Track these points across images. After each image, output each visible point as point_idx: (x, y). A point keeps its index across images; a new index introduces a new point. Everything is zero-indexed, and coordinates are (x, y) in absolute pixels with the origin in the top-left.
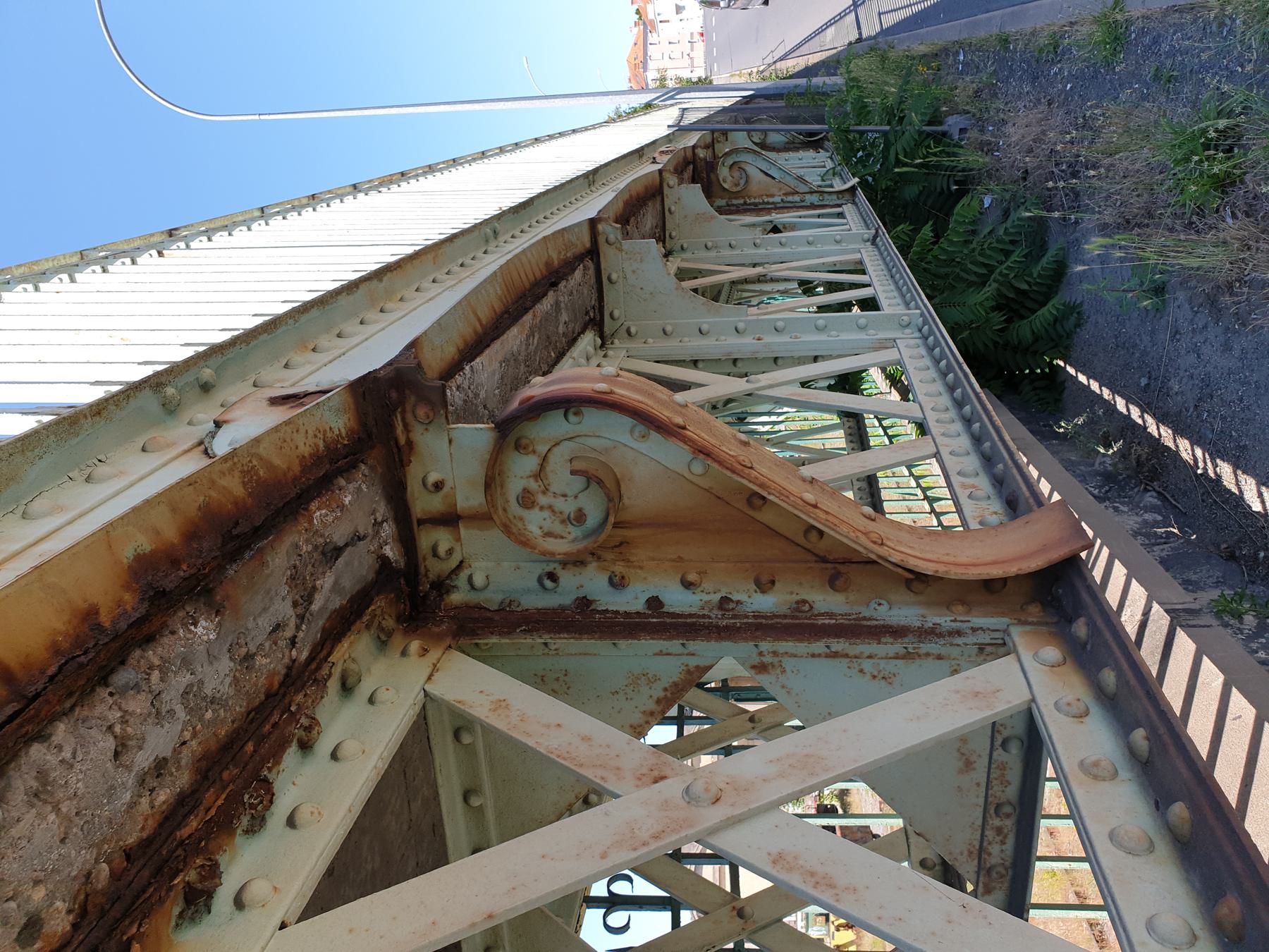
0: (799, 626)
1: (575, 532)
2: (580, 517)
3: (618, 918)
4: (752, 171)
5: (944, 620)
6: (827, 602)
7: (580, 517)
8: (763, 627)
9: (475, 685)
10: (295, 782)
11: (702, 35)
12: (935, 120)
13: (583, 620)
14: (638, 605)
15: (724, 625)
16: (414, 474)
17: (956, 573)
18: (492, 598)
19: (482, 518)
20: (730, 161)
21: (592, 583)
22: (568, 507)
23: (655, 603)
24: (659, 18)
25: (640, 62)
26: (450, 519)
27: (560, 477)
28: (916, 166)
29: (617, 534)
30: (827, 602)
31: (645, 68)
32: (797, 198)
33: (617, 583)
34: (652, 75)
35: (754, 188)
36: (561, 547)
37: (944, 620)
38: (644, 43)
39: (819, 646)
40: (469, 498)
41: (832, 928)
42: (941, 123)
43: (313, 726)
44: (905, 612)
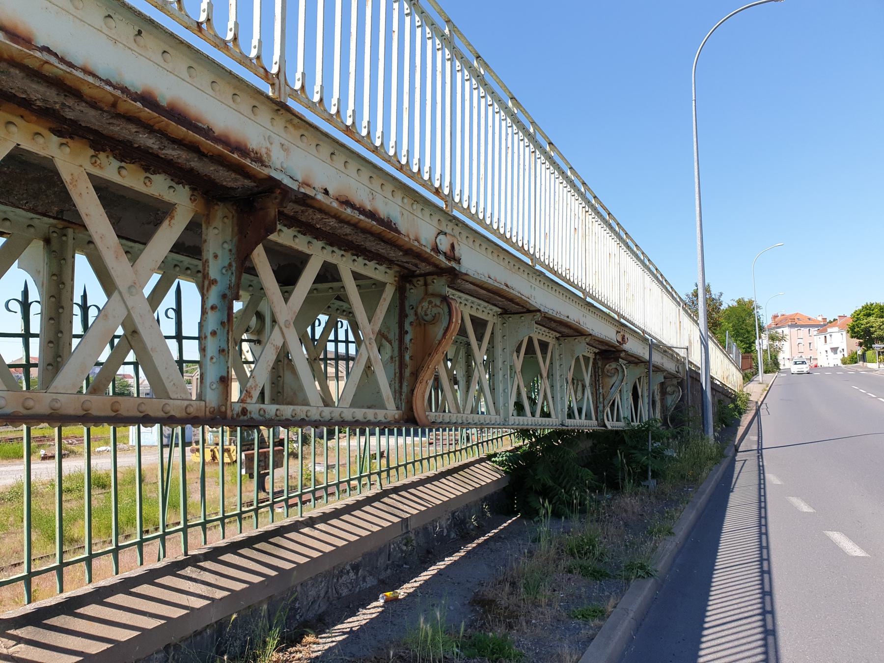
0: (402, 365)
1: (423, 314)
2: (426, 315)
3: (172, 314)
4: (615, 378)
5: (403, 397)
6: (407, 372)
7: (426, 315)
8: (401, 340)
9: (389, 293)
10: (372, 264)
11: (816, 366)
12: (655, 475)
13: (403, 316)
14: (406, 329)
15: (402, 349)
16: (435, 277)
17: (414, 399)
18: (407, 294)
19: (426, 293)
20: (619, 368)
21: (411, 318)
22: (429, 312)
23: (407, 332)
24: (828, 336)
25: (795, 323)
26: (426, 284)
27: (435, 311)
28: (622, 460)
29: (423, 324)
30: (407, 372)
31: (791, 326)
32: (601, 400)
33: (411, 324)
34: (786, 330)
35: (607, 380)
36: (419, 310)
37: (403, 397)
38: (809, 324)
39: (397, 370)
40: (431, 289)
41: (212, 447)
42: (653, 477)
43: (381, 265)
44: (405, 389)
